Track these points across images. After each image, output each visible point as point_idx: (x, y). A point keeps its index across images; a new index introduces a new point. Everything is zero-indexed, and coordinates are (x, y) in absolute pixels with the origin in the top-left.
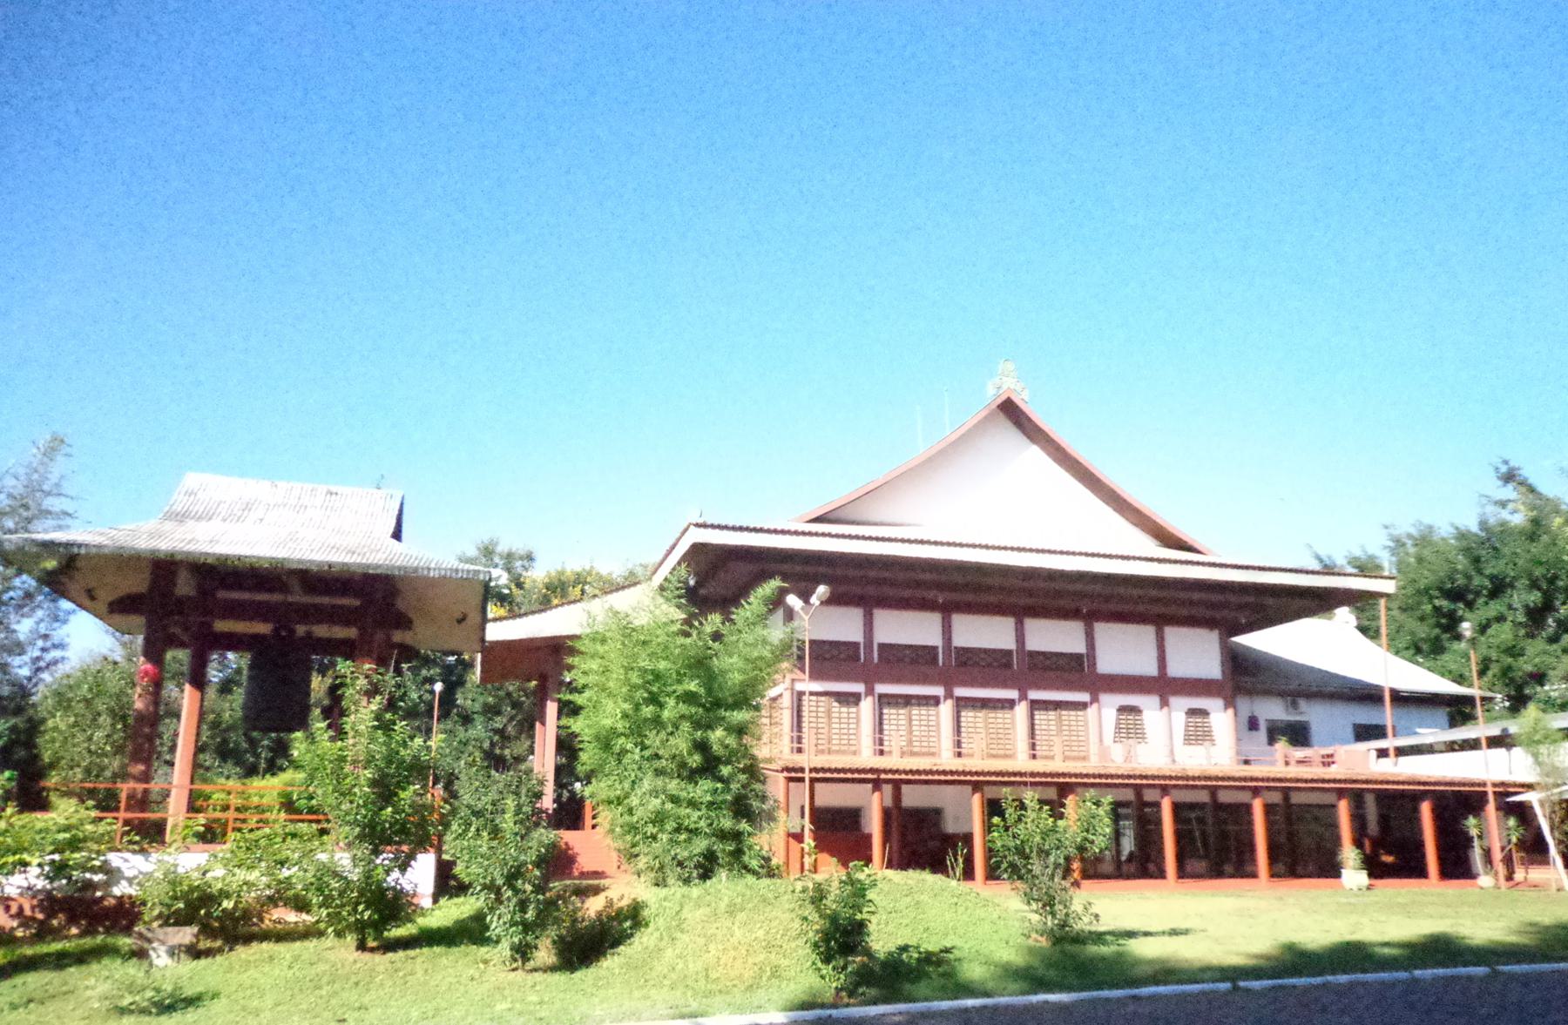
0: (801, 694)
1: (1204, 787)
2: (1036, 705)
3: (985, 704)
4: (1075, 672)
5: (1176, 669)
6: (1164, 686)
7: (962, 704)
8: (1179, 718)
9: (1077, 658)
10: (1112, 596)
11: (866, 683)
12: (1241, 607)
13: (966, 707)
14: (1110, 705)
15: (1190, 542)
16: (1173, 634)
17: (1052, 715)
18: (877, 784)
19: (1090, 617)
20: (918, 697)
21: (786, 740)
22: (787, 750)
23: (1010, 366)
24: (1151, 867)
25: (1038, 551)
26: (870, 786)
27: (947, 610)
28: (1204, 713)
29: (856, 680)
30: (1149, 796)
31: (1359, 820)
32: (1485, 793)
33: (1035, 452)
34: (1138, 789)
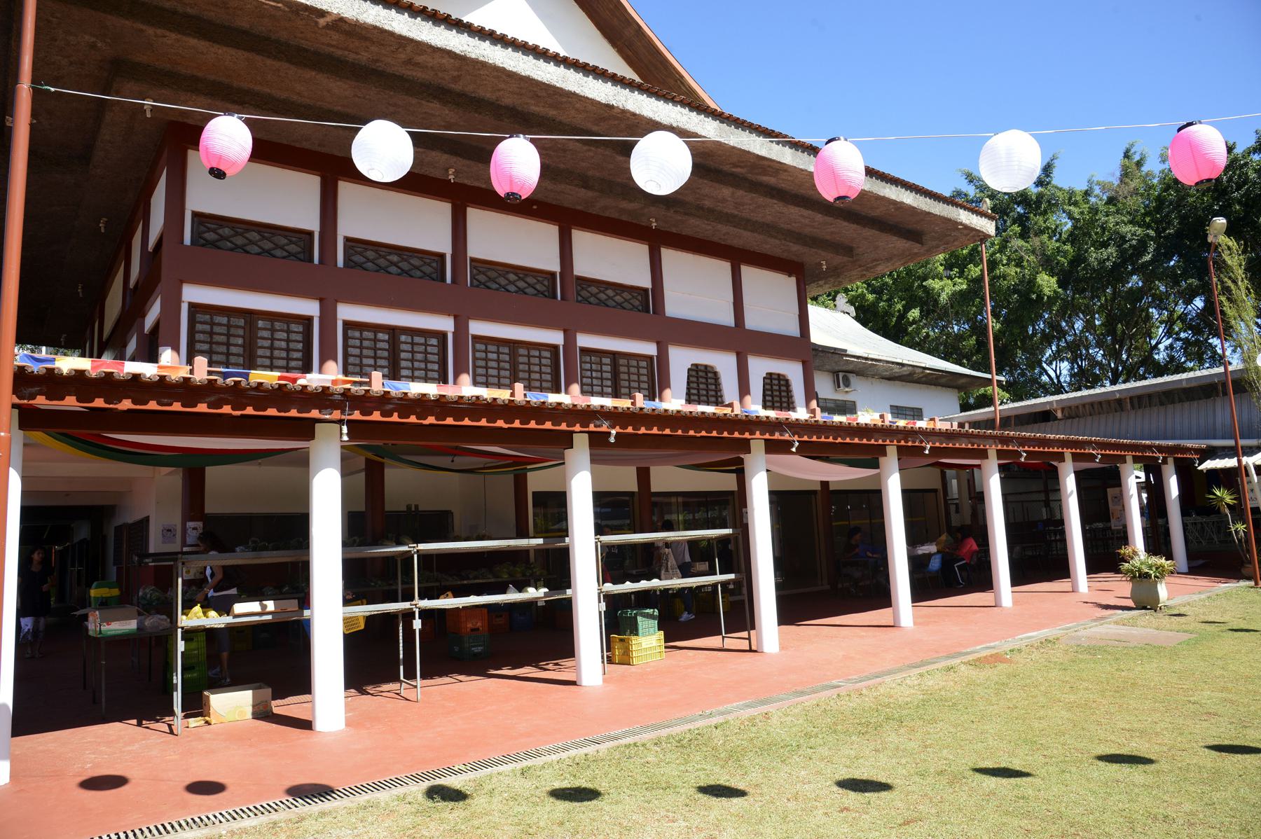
5: (755, 320)
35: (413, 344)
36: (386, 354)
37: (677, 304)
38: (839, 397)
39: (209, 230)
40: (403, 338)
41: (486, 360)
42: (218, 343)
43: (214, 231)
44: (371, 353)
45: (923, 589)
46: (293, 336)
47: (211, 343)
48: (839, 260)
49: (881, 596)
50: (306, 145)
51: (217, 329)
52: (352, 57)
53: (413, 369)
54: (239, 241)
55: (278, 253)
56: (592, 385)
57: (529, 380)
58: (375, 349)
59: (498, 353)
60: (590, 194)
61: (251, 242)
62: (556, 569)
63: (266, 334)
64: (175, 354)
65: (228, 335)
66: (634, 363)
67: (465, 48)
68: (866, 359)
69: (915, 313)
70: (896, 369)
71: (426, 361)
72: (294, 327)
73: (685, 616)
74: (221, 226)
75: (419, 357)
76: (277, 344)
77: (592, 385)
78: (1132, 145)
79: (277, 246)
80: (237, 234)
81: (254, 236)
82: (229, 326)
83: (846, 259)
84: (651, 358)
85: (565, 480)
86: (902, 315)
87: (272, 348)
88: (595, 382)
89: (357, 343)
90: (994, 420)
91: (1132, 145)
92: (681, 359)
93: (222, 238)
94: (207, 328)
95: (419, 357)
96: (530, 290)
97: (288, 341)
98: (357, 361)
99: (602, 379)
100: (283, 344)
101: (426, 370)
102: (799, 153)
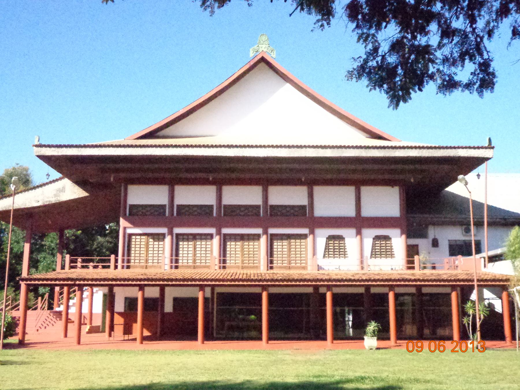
0: (130, 235)
1: (363, 286)
2: (273, 238)
3: (242, 237)
4: (302, 217)
5: (367, 211)
6: (359, 223)
7: (225, 239)
8: (368, 242)
9: (303, 207)
10: (356, 170)
11: (310, 228)
12: (410, 171)
13: (183, 240)
14: (322, 236)
15: (381, 134)
16: (365, 190)
17: (285, 243)
18: (202, 287)
19: (311, 183)
20: (201, 235)
21: (167, 261)
22: (167, 267)
23: (264, 38)
24: (321, 336)
25: (273, 146)
26: (138, 288)
27: (219, 184)
28: (387, 238)
29: (212, 226)
30: (322, 290)
31: (399, 304)
32: (474, 285)
33: (288, 86)
34: (316, 288)
37: (322, 210)
79: (147, 211)
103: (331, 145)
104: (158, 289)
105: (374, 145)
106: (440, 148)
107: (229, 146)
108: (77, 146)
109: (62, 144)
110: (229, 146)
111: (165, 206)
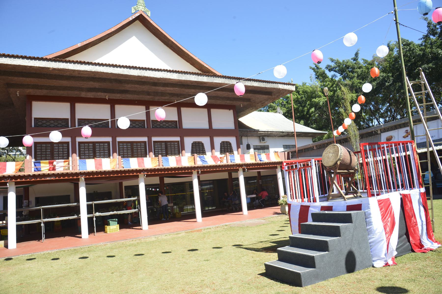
5: (216, 126)
6: (211, 132)
35: (100, 146)
36: (92, 149)
37: (187, 124)
38: (262, 144)
39: (39, 122)
40: (97, 144)
41: (123, 148)
42: (43, 152)
43: (41, 122)
44: (87, 150)
45: (251, 207)
46: (64, 148)
47: (41, 152)
48: (246, 103)
49: (240, 209)
50: (64, 95)
51: (43, 148)
52: (65, 74)
53: (100, 153)
54: (48, 124)
55: (59, 125)
56: (158, 152)
57: (123, 155)
58: (89, 149)
59: (127, 145)
60: (151, 97)
61: (51, 124)
62: (77, 210)
63: (57, 148)
64: (30, 157)
65: (46, 149)
66: (173, 143)
67: (91, 69)
68: (268, 132)
69: (313, 109)
70: (281, 134)
71: (104, 150)
72: (64, 145)
73: (163, 219)
74: (43, 121)
75: (102, 149)
76: (60, 150)
77: (158, 152)
78: (390, 42)
79: (59, 124)
80: (47, 122)
81: (52, 122)
82: (46, 147)
83: (248, 103)
84: (178, 141)
85: (138, 183)
86: (308, 110)
87: (58, 151)
88: (159, 150)
89: (83, 147)
90: (296, 151)
91: (390, 42)
92: (189, 141)
93: (43, 124)
94: (40, 148)
95: (102, 149)
96: (137, 126)
97: (63, 149)
98: (83, 152)
99: (162, 149)
100: (62, 150)
101: (104, 153)
102: (210, 77)
103: (124, 65)
104: (158, 178)
105: (224, 75)
106: (135, 68)
107: (130, 67)
108: (140, 68)
109: (19, 55)
110: (130, 67)
111: (67, 119)
